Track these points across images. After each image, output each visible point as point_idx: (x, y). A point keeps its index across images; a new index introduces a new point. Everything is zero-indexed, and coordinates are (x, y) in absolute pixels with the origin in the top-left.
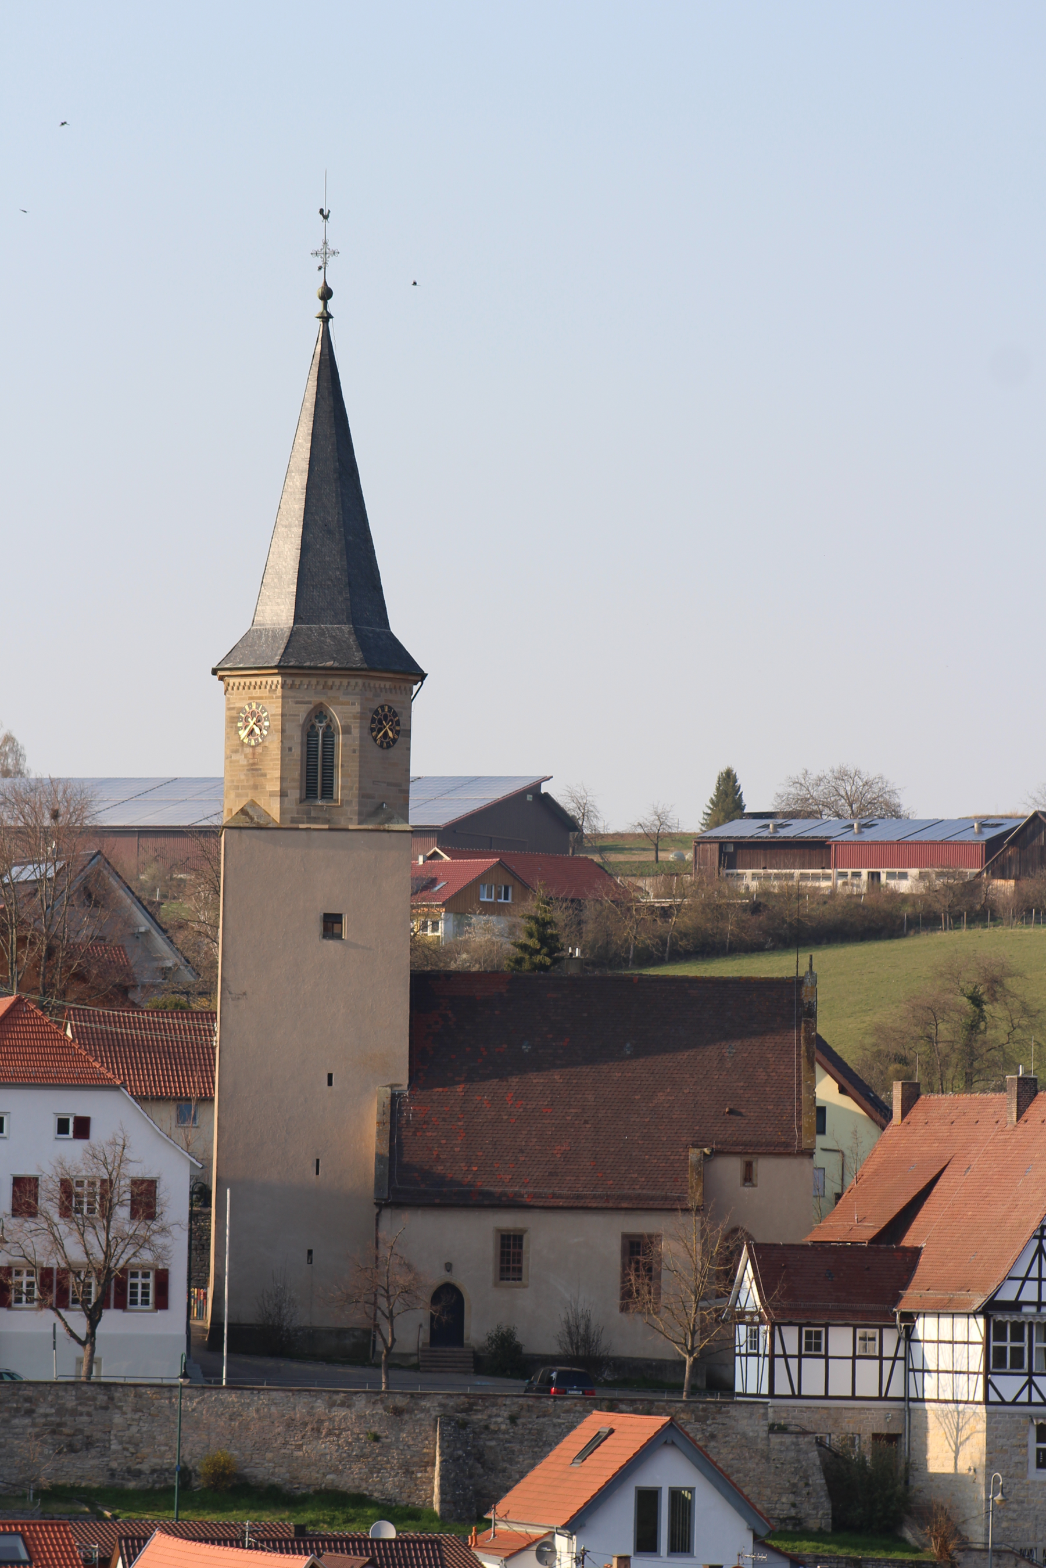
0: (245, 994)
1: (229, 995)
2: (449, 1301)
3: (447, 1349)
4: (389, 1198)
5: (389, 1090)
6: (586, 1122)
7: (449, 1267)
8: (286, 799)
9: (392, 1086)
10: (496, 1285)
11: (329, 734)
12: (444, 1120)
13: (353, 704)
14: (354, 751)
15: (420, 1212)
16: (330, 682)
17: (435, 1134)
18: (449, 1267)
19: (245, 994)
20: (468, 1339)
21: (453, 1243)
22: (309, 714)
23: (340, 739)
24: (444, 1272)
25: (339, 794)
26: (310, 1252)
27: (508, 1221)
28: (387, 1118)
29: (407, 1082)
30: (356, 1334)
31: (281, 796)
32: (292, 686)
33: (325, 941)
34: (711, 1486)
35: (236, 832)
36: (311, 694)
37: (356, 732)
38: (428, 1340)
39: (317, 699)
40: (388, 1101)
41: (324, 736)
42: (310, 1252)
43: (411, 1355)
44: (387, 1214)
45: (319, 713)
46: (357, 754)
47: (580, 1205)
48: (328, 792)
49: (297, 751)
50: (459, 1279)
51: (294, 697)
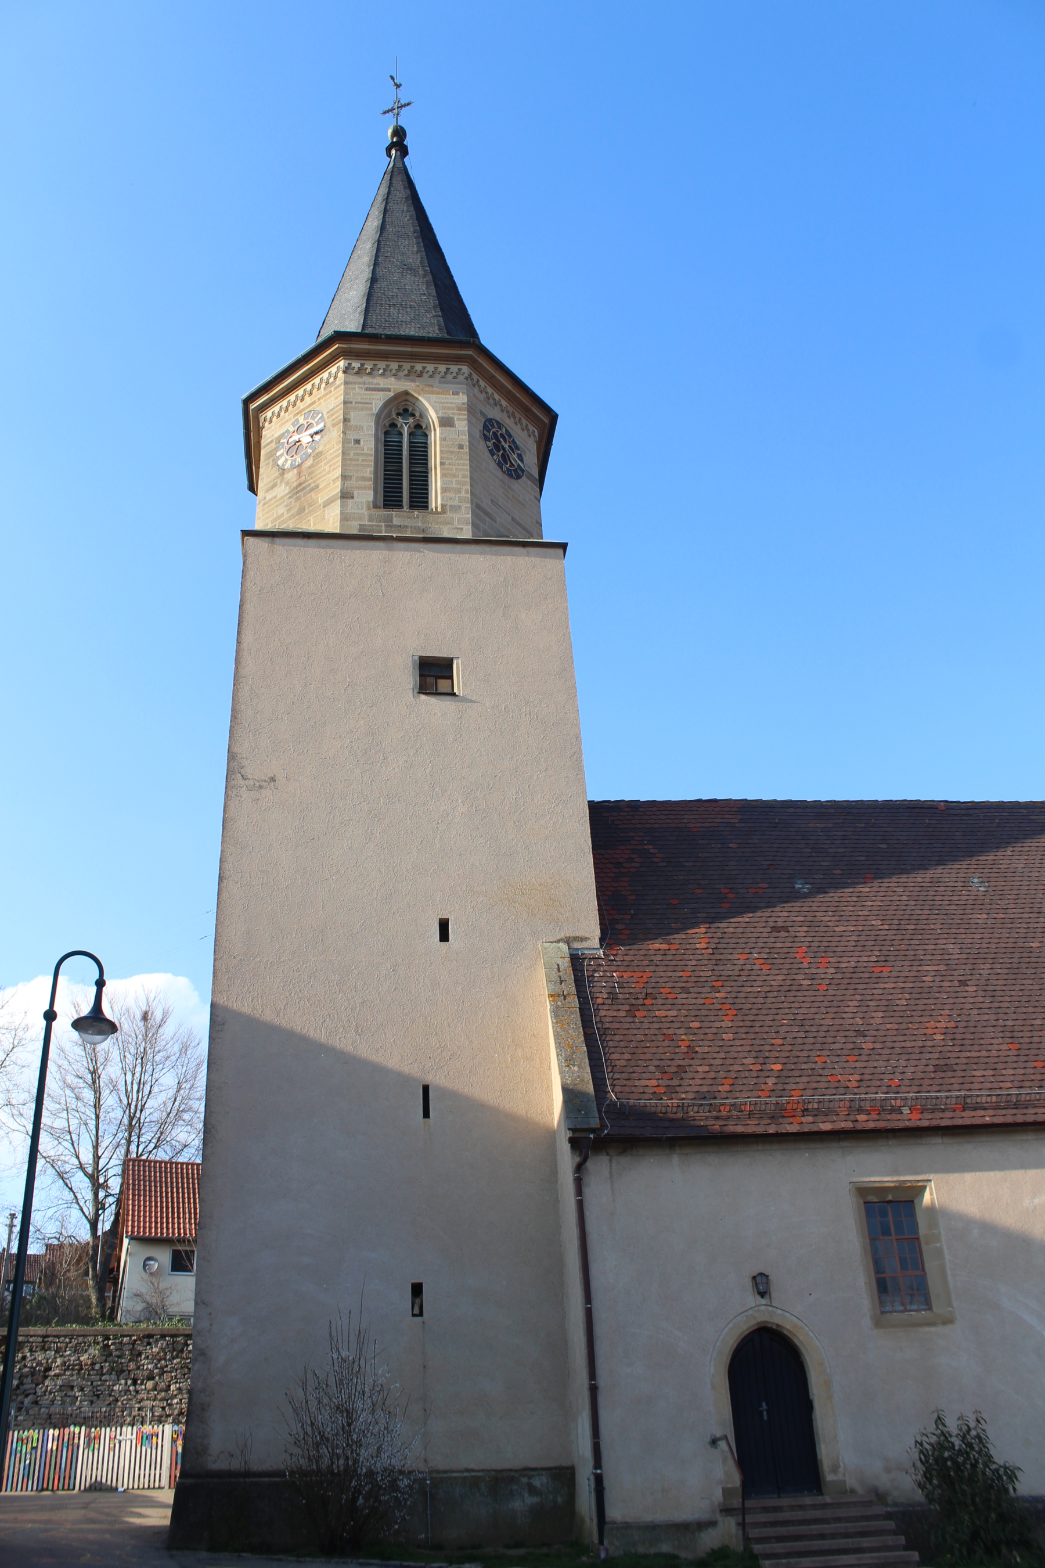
0: (273, 779)
1: (241, 782)
2: (768, 1376)
3: (785, 1501)
4: (603, 1126)
5: (564, 947)
6: (963, 983)
7: (761, 1285)
8: (350, 502)
9: (568, 941)
10: (878, 1324)
11: (420, 431)
12: (685, 990)
13: (457, 393)
14: (461, 447)
15: (676, 1159)
16: (419, 367)
17: (674, 1013)
18: (761, 1285)
19: (273, 779)
20: (835, 1469)
21: (774, 1227)
22: (386, 404)
23: (436, 438)
24: (752, 1300)
25: (436, 498)
26: (417, 1290)
27: (880, 1168)
28: (571, 988)
29: (598, 933)
30: (537, 1482)
31: (342, 497)
32: (360, 372)
33: (423, 697)
34: (577, 1486)
35: (263, 544)
36: (385, 385)
37: (462, 425)
38: (736, 1480)
39: (396, 385)
40: (566, 963)
41: (411, 434)
42: (417, 1290)
43: (702, 1526)
44: (599, 1166)
45: (402, 409)
46: (466, 450)
47: (1030, 1119)
48: (420, 500)
49: (369, 444)
50: (792, 1314)
51: (364, 383)
